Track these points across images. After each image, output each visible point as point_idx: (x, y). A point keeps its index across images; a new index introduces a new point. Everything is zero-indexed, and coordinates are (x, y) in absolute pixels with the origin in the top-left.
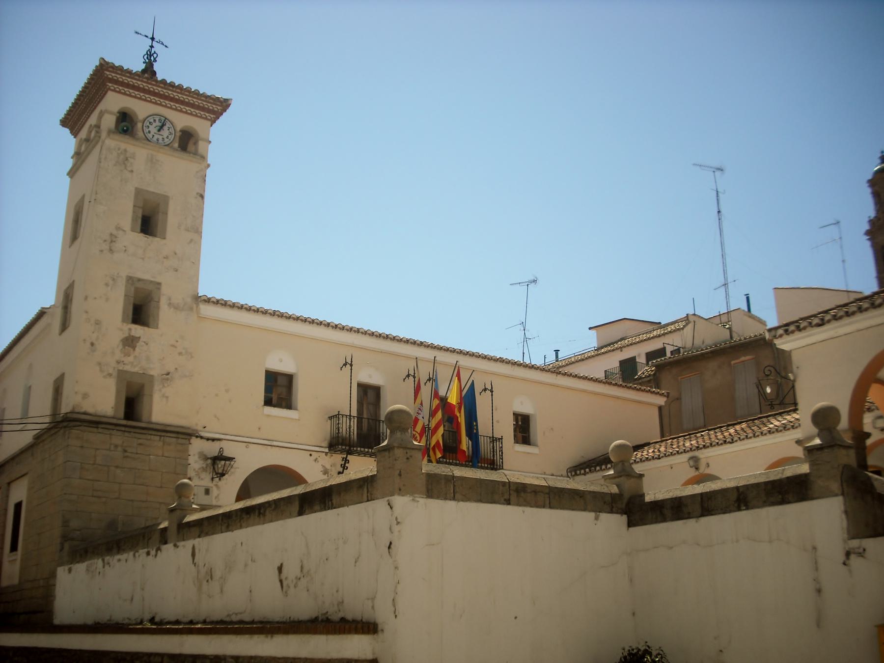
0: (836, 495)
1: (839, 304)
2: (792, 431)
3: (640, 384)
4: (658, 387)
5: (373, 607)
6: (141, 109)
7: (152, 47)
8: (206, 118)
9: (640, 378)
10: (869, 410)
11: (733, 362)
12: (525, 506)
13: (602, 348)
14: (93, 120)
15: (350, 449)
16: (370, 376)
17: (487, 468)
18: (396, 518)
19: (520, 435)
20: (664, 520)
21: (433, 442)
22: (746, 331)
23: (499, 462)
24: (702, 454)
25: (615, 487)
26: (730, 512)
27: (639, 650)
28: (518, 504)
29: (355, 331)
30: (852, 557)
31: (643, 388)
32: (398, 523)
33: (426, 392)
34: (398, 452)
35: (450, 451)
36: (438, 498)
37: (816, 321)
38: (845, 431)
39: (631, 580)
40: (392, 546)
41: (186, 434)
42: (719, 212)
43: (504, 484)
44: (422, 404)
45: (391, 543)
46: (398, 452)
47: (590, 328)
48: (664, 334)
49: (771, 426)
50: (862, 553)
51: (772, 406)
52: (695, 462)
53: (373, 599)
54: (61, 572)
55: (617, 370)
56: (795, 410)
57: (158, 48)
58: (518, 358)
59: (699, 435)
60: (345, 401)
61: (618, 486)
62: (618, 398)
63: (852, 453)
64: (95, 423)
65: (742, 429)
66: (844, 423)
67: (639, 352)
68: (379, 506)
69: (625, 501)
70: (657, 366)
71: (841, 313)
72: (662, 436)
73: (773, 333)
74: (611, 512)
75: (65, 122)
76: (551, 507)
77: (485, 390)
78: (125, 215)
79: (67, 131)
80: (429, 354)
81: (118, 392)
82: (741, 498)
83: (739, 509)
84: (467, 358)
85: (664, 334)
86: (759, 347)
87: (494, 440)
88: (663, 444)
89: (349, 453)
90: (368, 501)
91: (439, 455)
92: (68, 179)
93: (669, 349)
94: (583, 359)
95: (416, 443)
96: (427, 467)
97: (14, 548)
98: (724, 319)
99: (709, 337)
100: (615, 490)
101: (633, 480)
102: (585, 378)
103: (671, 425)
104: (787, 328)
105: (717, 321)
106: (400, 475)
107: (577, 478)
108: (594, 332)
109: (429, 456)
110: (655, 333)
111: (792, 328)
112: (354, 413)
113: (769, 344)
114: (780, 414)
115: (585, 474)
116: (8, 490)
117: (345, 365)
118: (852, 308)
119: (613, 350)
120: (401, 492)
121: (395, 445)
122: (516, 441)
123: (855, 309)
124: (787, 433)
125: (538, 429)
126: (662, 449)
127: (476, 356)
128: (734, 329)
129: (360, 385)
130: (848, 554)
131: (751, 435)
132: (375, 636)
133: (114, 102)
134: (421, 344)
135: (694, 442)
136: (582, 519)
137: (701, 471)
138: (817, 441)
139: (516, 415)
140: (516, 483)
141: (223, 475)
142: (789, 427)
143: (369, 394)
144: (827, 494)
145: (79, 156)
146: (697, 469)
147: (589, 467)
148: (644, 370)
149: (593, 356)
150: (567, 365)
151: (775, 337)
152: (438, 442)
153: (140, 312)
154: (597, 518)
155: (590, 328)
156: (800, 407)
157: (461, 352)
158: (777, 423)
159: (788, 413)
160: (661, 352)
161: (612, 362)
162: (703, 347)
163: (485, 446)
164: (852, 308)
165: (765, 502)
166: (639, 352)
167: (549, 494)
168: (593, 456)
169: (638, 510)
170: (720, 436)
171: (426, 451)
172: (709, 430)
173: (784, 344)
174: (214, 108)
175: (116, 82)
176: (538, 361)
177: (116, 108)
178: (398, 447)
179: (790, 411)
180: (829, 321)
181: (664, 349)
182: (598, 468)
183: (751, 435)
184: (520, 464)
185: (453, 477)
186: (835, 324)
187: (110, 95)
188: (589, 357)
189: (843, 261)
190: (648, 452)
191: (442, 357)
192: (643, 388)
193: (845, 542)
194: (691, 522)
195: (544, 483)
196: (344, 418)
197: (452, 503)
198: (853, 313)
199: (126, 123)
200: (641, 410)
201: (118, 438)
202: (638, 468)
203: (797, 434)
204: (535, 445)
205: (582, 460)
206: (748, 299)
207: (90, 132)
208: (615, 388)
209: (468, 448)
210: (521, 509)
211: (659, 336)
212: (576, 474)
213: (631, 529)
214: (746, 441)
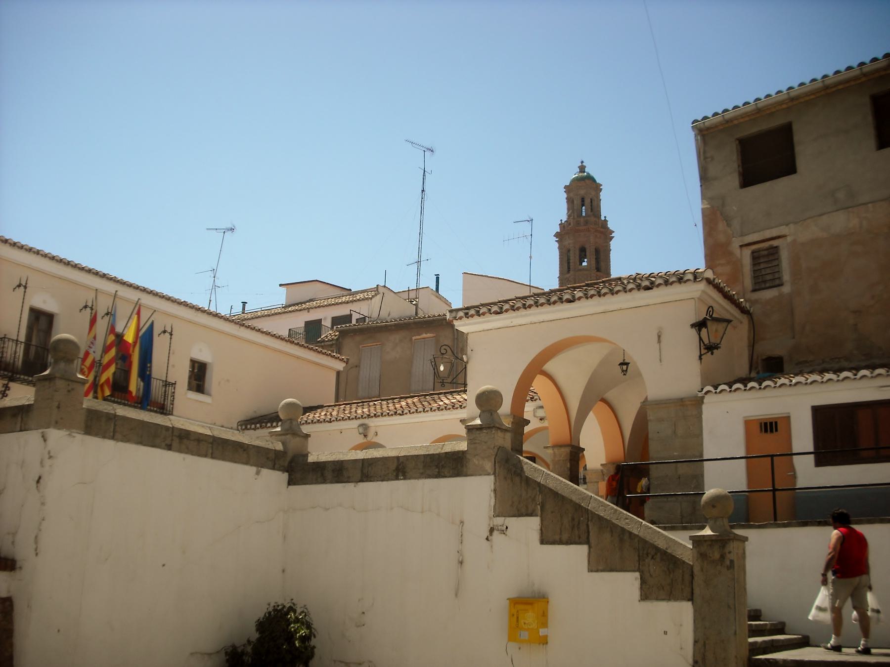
0: (489, 474)
1: (518, 296)
2: (459, 410)
3: (322, 347)
4: (339, 352)
5: (13, 543)
9: (323, 341)
10: (532, 399)
11: (414, 338)
12: (186, 453)
13: (290, 306)
15: (12, 376)
16: (44, 302)
17: (156, 412)
18: (49, 453)
19: (194, 383)
20: (324, 481)
21: (103, 378)
22: (431, 309)
23: (169, 407)
24: (373, 423)
25: (280, 444)
26: (388, 480)
27: (284, 607)
28: (180, 451)
29: (34, 252)
30: (495, 533)
31: (324, 351)
32: (50, 457)
33: (102, 325)
34: (60, 384)
35: (119, 389)
36: (96, 435)
37: (495, 308)
38: (506, 416)
39: (285, 537)
40: (41, 481)
42: (423, 191)
43: (167, 428)
44: (95, 338)
45: (40, 478)
46: (60, 384)
47: (281, 285)
48: (352, 301)
49: (441, 403)
50: (504, 531)
51: (443, 384)
52: (365, 430)
53: (14, 534)
55: (302, 331)
56: (465, 391)
58: (204, 305)
59: (371, 404)
61: (283, 444)
62: (298, 358)
63: (508, 436)
65: (414, 403)
66: (505, 408)
67: (326, 316)
68: (32, 438)
69: (288, 459)
70: (340, 332)
71: (519, 305)
72: (337, 400)
73: (454, 314)
74: (273, 468)
76: (213, 457)
77: (165, 332)
80: (111, 287)
82: (400, 468)
83: (397, 478)
84: (150, 297)
85: (352, 301)
86: (440, 325)
87: (167, 384)
88: (336, 408)
89: (12, 379)
90: (21, 431)
91: (107, 392)
93: (355, 317)
94: (270, 314)
95: (80, 376)
96: (89, 402)
98: (412, 295)
99: (398, 310)
100: (279, 447)
101: (298, 439)
102: (268, 334)
103: (346, 391)
104: (468, 312)
105: (406, 296)
106: (58, 407)
107: (246, 432)
108: (284, 289)
109: (96, 392)
110: (344, 299)
111: (472, 312)
112: (22, 338)
113: (450, 325)
114: (451, 393)
115: (255, 429)
117: (19, 286)
118: (530, 302)
119: (300, 310)
120: (58, 425)
121: (57, 375)
122: (190, 388)
123: (532, 302)
124: (455, 411)
125: (214, 379)
126: (334, 413)
127: (160, 297)
128: (419, 306)
130: (492, 530)
131: (421, 409)
132: (12, 573)
134: (104, 276)
135: (365, 410)
136: (241, 474)
137: (369, 438)
138: (478, 422)
139: (193, 362)
140: (333, 462)
142: (456, 406)
144: (481, 472)
146: (365, 436)
147: (260, 422)
148: (328, 333)
149: (280, 313)
150: (253, 318)
151: (455, 318)
152: (108, 380)
154: (258, 473)
155: (281, 285)
156: (468, 388)
157: (144, 290)
158: (447, 401)
159: (458, 393)
160: (347, 318)
161: (298, 322)
162: (389, 319)
163: (156, 388)
164: (530, 302)
165: (422, 474)
166: (326, 316)
167: (212, 443)
168: (266, 413)
169: (299, 469)
170: (391, 407)
171: (95, 387)
172: (382, 400)
173: (462, 326)
176: (224, 311)
178: (61, 378)
179: (461, 391)
180: (507, 311)
181: (351, 315)
182: (269, 425)
184: (191, 412)
185: (115, 416)
186: (511, 314)
188: (276, 314)
189: (531, 257)
190: (320, 414)
191: (123, 292)
192: (324, 351)
193: (490, 518)
194: (351, 486)
195: (208, 433)
196: (11, 343)
197: (110, 443)
198: (530, 306)
200: (319, 372)
202: (305, 429)
203: (463, 414)
204: (209, 394)
205: (254, 415)
206: (438, 279)
208: (297, 347)
209: (138, 390)
210: (183, 455)
211: (348, 302)
212: (246, 429)
213: (290, 487)
214: (415, 415)
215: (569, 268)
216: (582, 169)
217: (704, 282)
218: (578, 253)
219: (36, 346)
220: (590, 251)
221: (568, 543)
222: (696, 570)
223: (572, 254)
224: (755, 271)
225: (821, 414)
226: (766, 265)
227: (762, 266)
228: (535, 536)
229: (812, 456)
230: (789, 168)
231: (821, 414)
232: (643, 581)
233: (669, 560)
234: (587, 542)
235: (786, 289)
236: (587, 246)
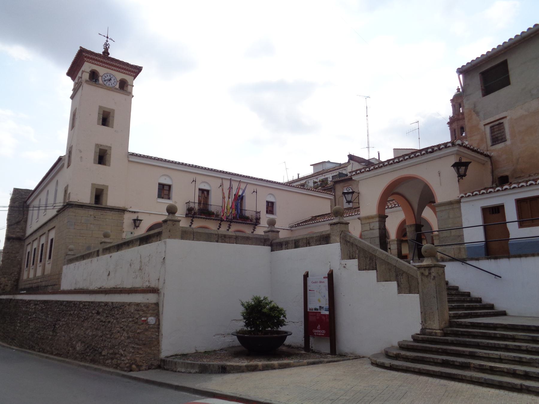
6: (102, 71)
7: (107, 41)
8: (131, 75)
14: (79, 75)
41: (123, 211)
54: (65, 267)
57: (110, 42)
60: (194, 198)
64: (81, 206)
75: (69, 74)
78: (95, 117)
79: (69, 78)
81: (92, 193)
92: (71, 100)
97: (50, 258)
112: (197, 201)
116: (48, 234)
129: (200, 189)
133: (87, 67)
141: (138, 226)
143: (205, 193)
145: (76, 90)
153: (102, 157)
174: (136, 70)
175: (88, 58)
177: (89, 70)
183: (390, 207)
187: (86, 64)
199: (94, 76)
201: (91, 212)
207: (79, 80)
215: (456, 137)
217: (458, 146)
218: (459, 130)
221: (369, 269)
222: (420, 280)
224: (492, 136)
225: (519, 202)
226: (498, 132)
227: (496, 133)
228: (356, 268)
229: (482, 228)
230: (506, 82)
231: (519, 202)
232: (399, 285)
233: (410, 277)
234: (376, 269)
235: (508, 142)
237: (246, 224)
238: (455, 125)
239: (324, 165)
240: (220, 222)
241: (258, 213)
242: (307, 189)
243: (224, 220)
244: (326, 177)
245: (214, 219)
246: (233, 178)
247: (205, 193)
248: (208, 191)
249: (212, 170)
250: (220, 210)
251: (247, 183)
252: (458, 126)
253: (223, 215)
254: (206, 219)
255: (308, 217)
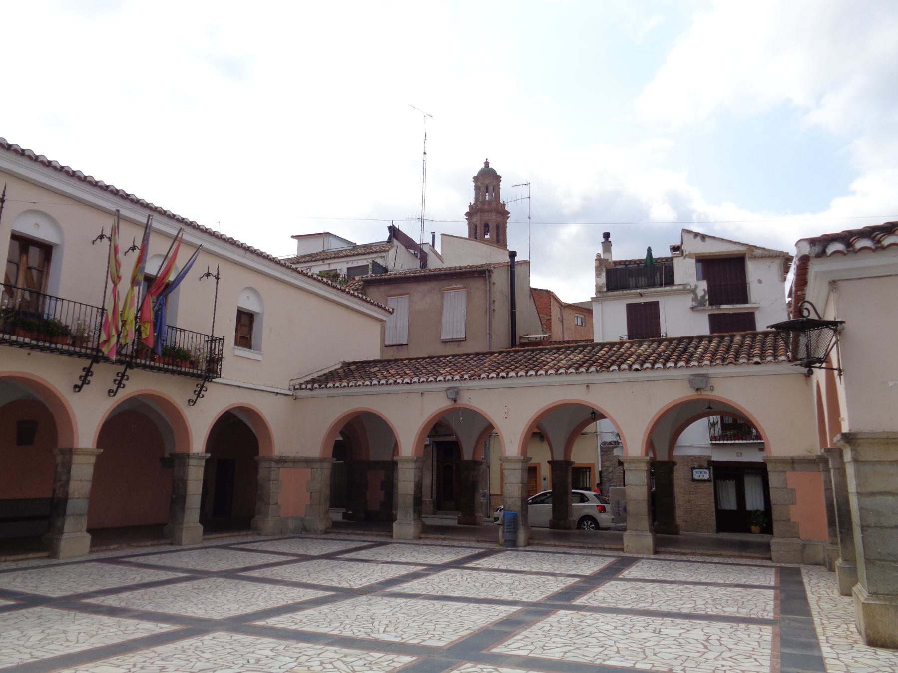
47: (293, 237)
108: (296, 241)
125: (265, 331)
155: (293, 237)
204: (259, 349)
206: (433, 236)
216: (487, 163)
219: (24, 289)
220: (492, 227)
223: (479, 229)
236: (490, 224)
237: (52, 351)
238: (475, 219)
239: (326, 239)
240: (87, 363)
241: (212, 340)
242: (384, 309)
243: (107, 360)
244: (332, 267)
245: (62, 352)
246: (188, 236)
247: (35, 254)
248: (47, 250)
249: (62, 170)
250: (92, 320)
251: (198, 248)
252: (481, 220)
253: (107, 342)
254: (32, 347)
255: (333, 364)
